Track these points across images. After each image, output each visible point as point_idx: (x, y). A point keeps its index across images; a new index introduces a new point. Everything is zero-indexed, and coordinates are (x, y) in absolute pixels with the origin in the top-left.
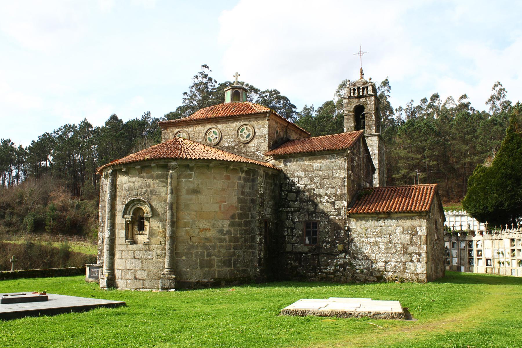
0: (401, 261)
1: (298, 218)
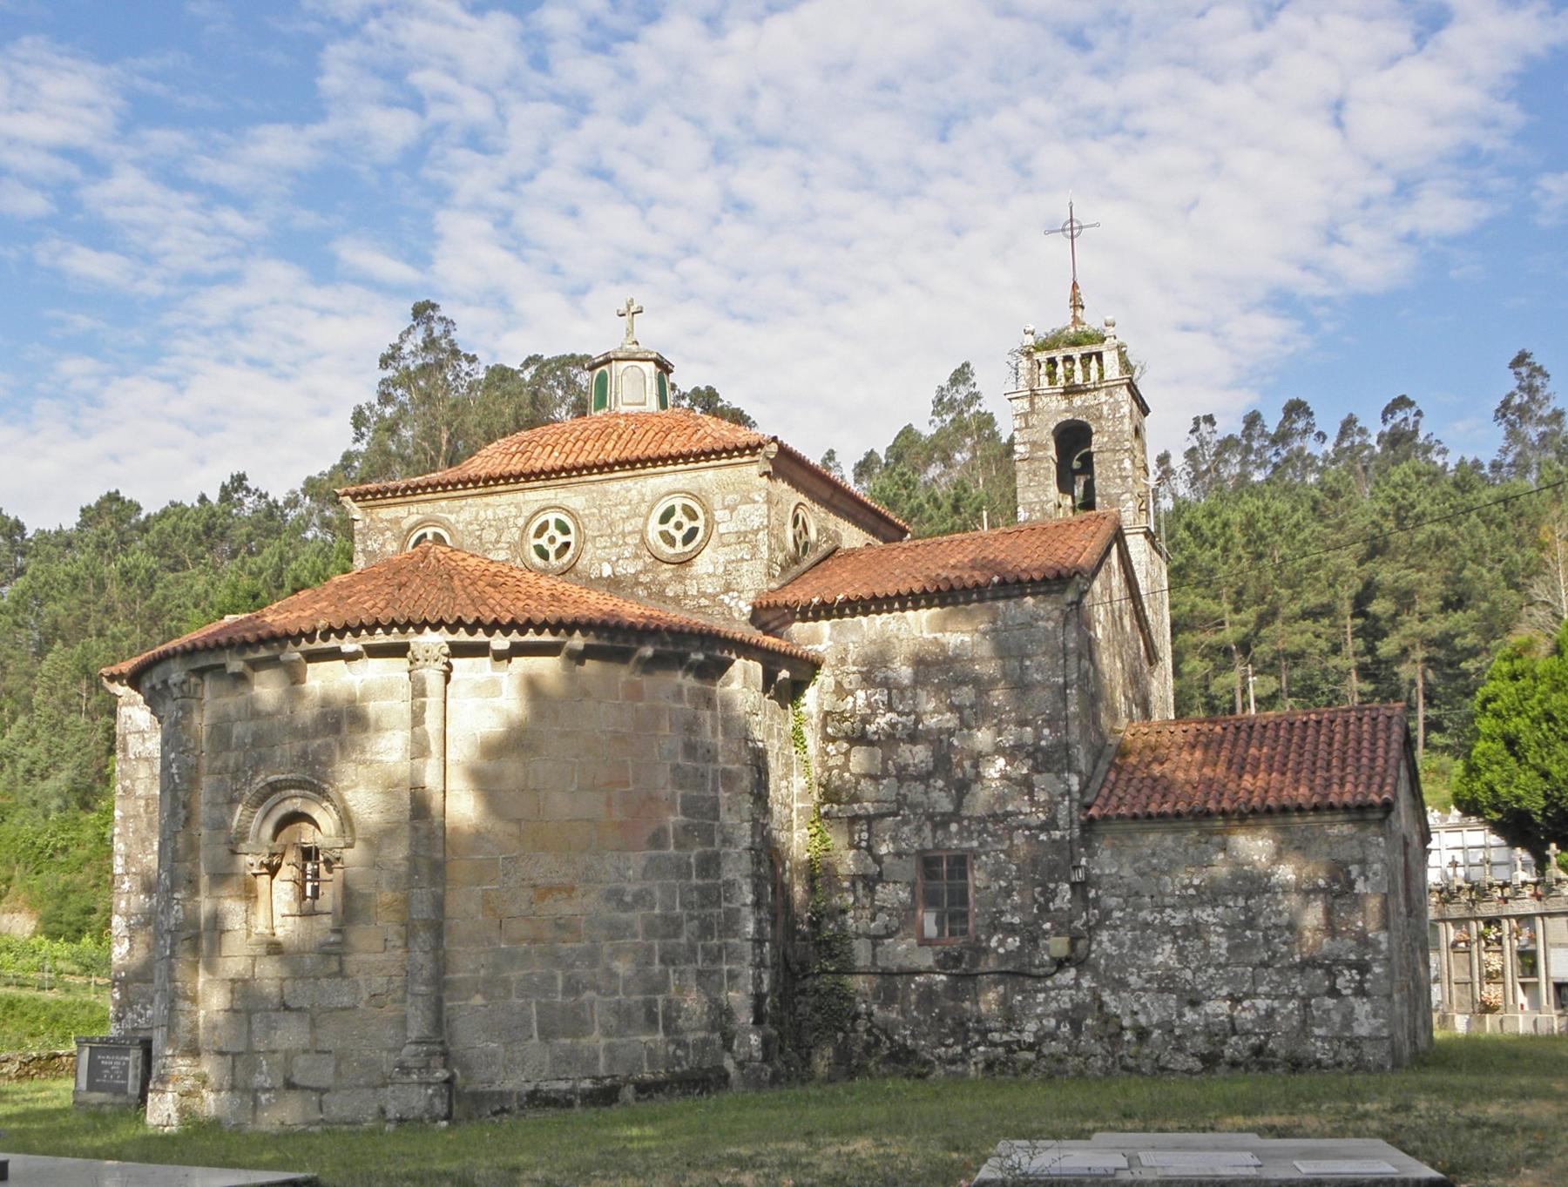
0: (1294, 995)
1: (894, 839)
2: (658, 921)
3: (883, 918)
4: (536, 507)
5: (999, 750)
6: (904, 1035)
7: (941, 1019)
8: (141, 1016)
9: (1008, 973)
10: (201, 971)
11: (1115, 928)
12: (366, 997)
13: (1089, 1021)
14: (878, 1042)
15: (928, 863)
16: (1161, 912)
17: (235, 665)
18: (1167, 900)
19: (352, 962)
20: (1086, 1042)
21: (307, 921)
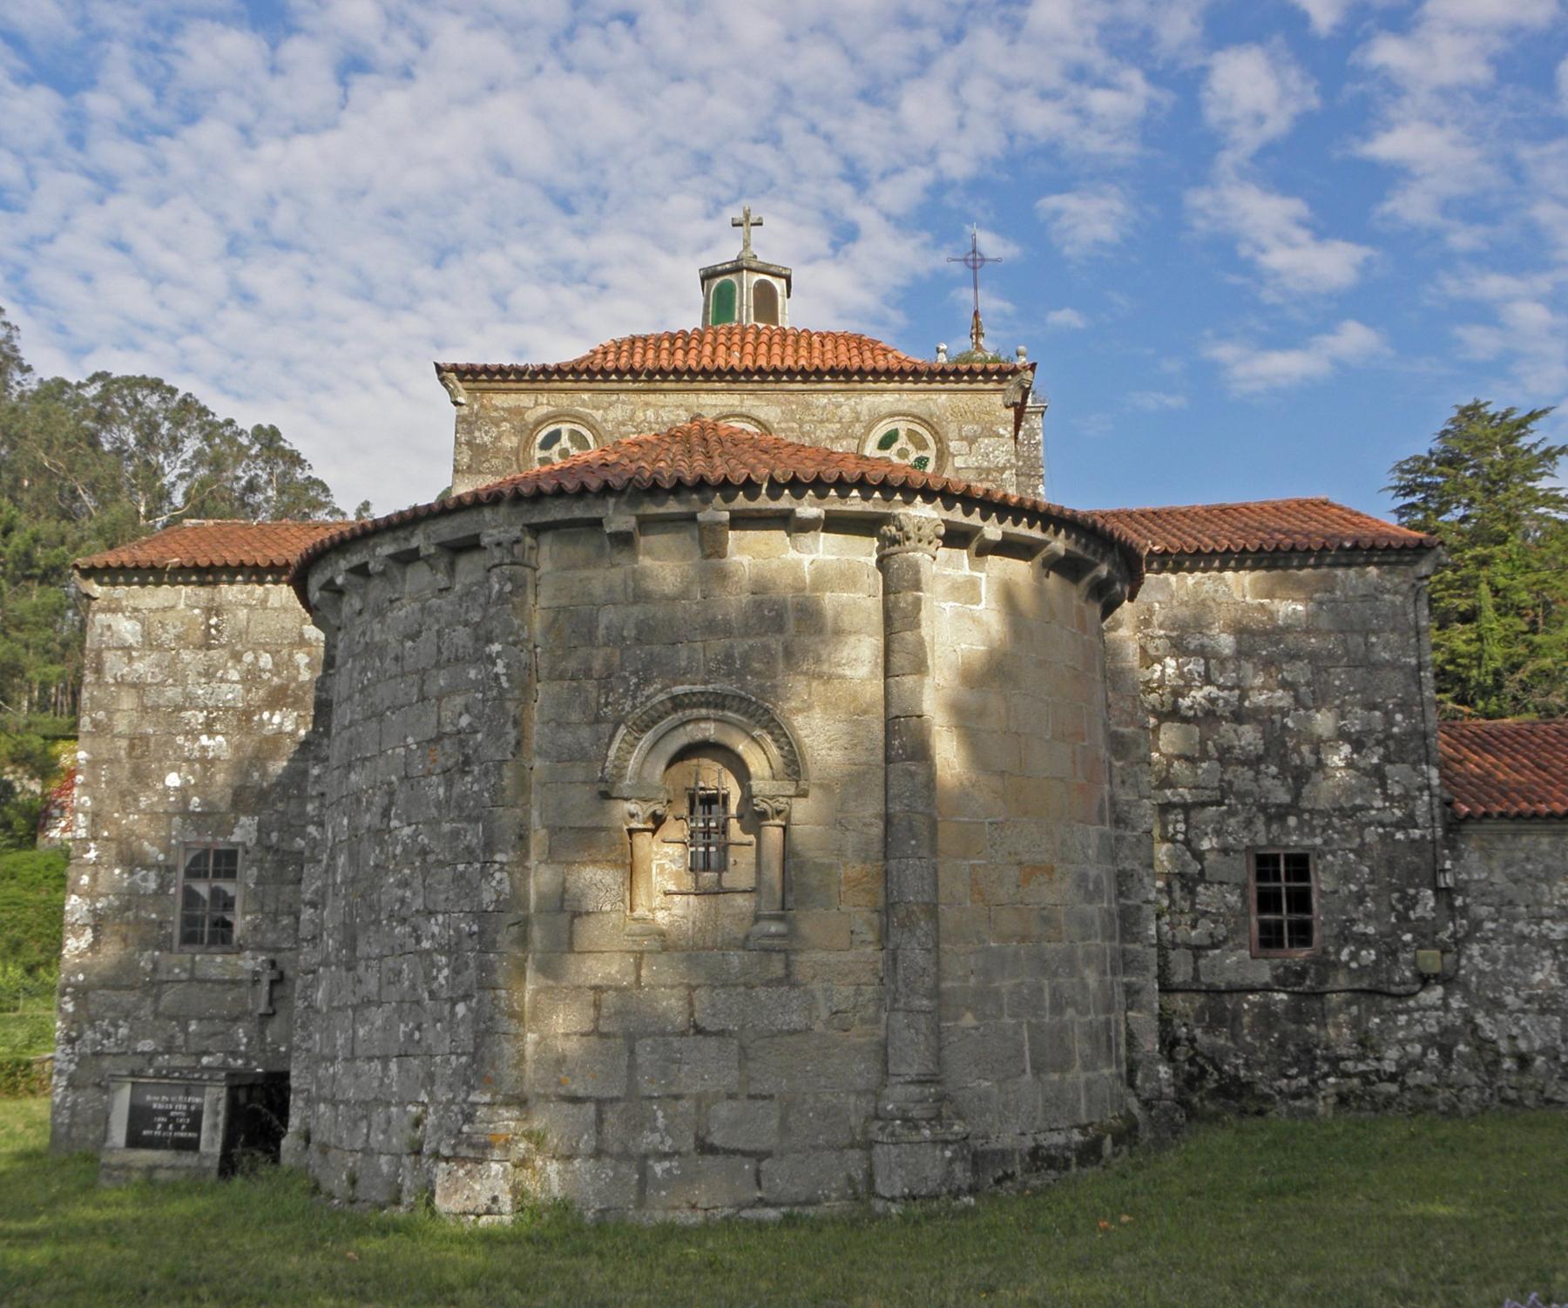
1: (1218, 833)
3: (1205, 925)
5: (1343, 735)
6: (1235, 1064)
7: (1281, 1045)
8: (108, 1035)
9: (1362, 991)
10: (529, 974)
11: (1487, 940)
12: (825, 1014)
13: (1461, 1047)
14: (1203, 1071)
15: (1265, 864)
16: (1538, 924)
17: (620, 519)
18: (1546, 910)
19: (805, 962)
21: (705, 902)
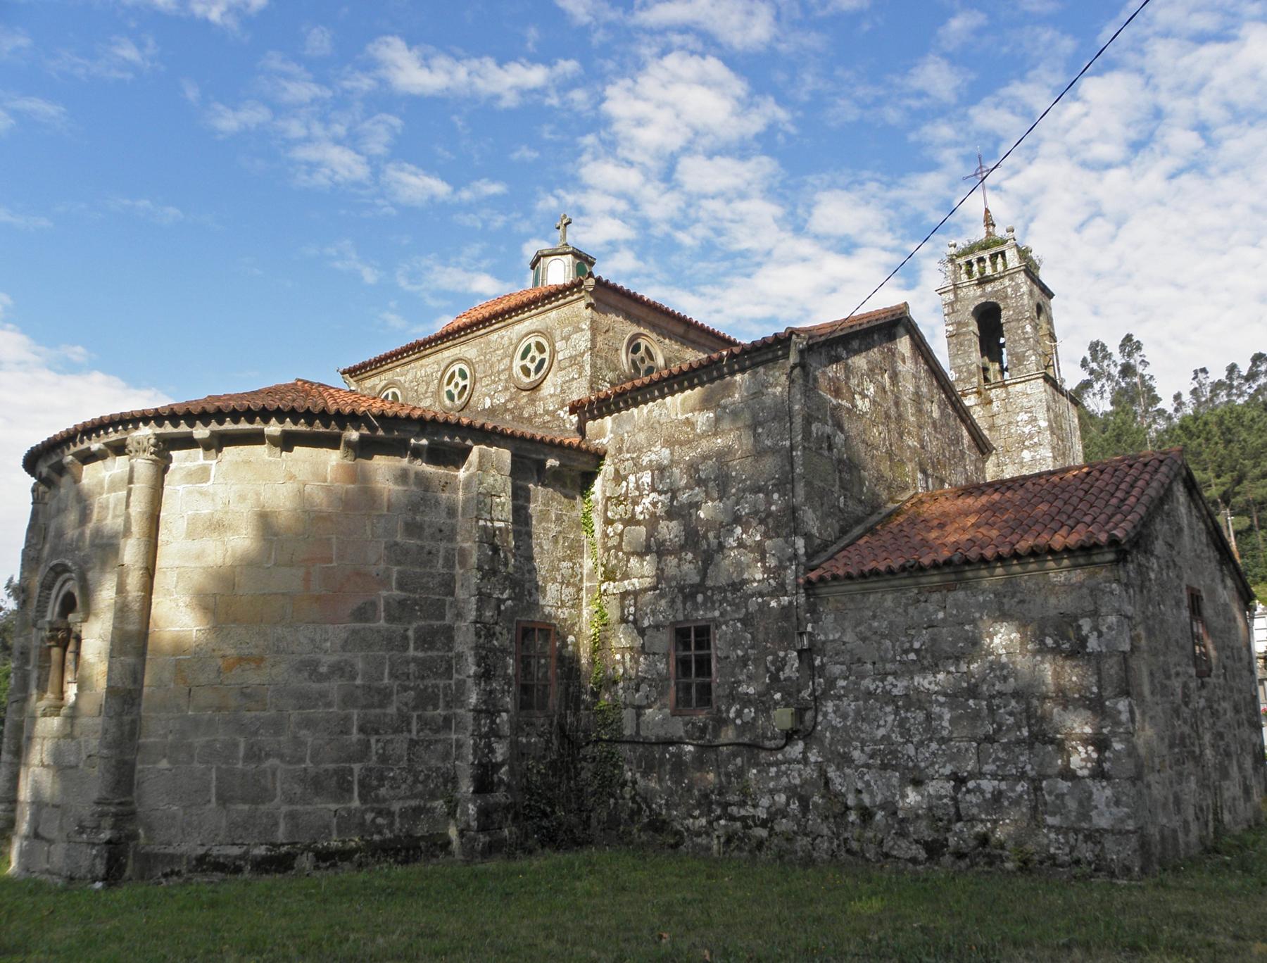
0: (1022, 776)
2: (359, 692)
4: (447, 361)
11: (839, 698)
12: (84, 757)
16: (882, 681)
18: (889, 667)
20: (813, 820)
